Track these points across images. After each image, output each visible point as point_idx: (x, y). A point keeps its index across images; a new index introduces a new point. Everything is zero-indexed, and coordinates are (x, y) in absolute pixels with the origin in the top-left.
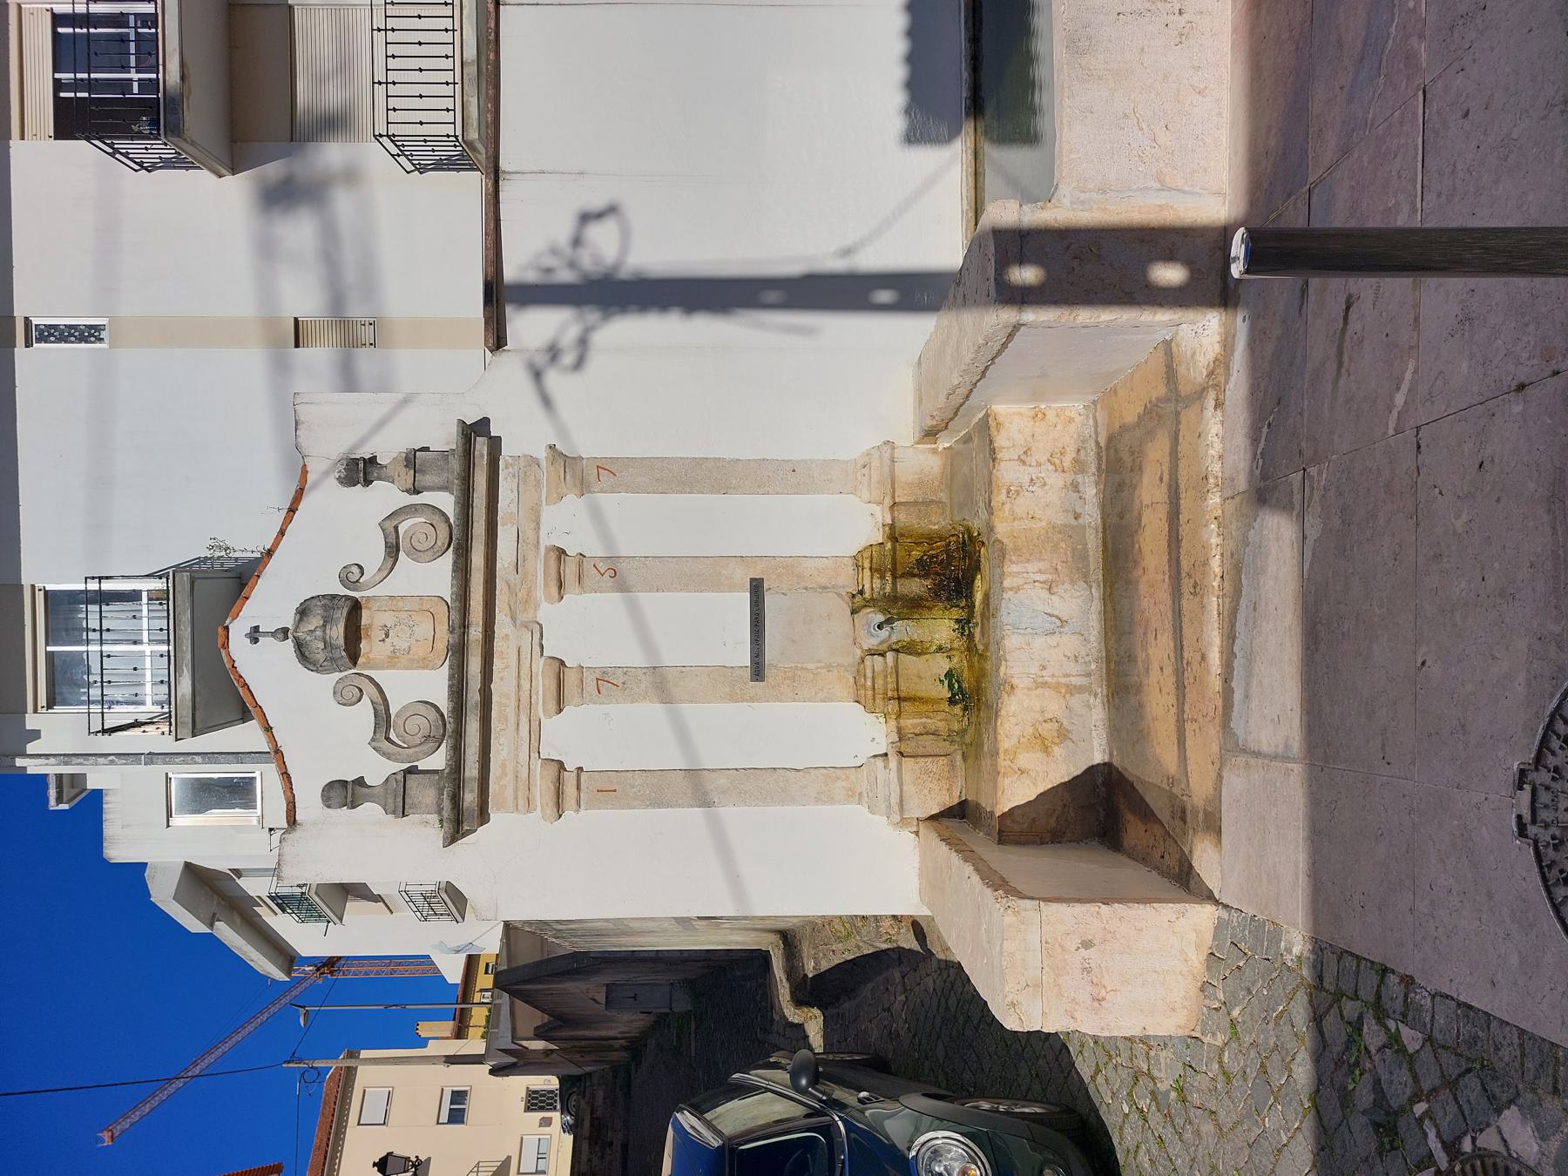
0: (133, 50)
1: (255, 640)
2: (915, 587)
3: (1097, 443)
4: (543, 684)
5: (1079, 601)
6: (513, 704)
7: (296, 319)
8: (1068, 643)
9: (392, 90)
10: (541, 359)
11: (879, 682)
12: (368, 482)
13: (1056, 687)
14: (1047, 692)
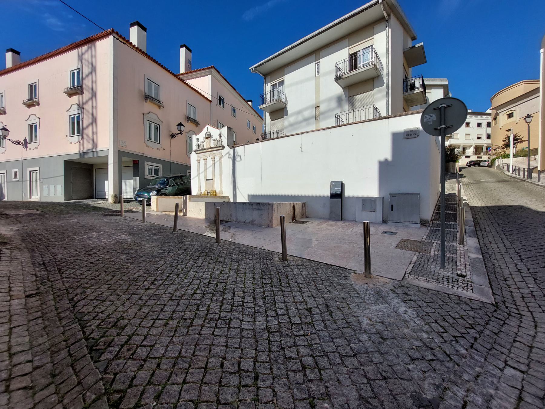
4: (205, 158)
9: (343, 115)
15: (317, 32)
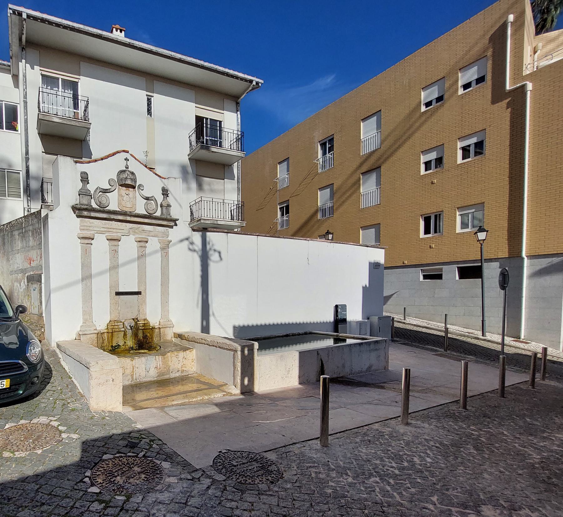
0: (213, 139)
1: (125, 160)
2: (140, 335)
3: (188, 375)
4: (114, 235)
5: (153, 375)
6: (110, 227)
7: (154, 169)
8: (143, 374)
10: (190, 240)
11: (116, 327)
12: (163, 194)
13: (133, 372)
14: (132, 369)
15: (178, 56)
